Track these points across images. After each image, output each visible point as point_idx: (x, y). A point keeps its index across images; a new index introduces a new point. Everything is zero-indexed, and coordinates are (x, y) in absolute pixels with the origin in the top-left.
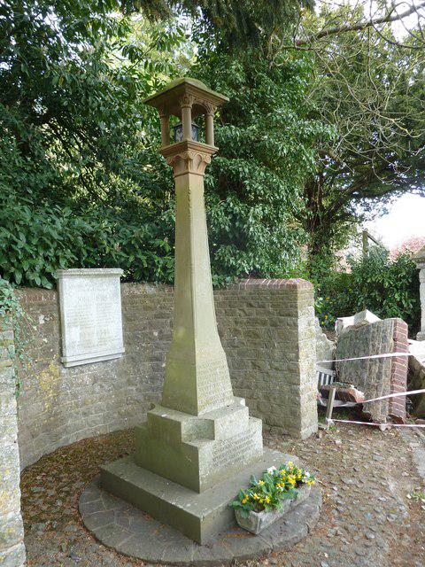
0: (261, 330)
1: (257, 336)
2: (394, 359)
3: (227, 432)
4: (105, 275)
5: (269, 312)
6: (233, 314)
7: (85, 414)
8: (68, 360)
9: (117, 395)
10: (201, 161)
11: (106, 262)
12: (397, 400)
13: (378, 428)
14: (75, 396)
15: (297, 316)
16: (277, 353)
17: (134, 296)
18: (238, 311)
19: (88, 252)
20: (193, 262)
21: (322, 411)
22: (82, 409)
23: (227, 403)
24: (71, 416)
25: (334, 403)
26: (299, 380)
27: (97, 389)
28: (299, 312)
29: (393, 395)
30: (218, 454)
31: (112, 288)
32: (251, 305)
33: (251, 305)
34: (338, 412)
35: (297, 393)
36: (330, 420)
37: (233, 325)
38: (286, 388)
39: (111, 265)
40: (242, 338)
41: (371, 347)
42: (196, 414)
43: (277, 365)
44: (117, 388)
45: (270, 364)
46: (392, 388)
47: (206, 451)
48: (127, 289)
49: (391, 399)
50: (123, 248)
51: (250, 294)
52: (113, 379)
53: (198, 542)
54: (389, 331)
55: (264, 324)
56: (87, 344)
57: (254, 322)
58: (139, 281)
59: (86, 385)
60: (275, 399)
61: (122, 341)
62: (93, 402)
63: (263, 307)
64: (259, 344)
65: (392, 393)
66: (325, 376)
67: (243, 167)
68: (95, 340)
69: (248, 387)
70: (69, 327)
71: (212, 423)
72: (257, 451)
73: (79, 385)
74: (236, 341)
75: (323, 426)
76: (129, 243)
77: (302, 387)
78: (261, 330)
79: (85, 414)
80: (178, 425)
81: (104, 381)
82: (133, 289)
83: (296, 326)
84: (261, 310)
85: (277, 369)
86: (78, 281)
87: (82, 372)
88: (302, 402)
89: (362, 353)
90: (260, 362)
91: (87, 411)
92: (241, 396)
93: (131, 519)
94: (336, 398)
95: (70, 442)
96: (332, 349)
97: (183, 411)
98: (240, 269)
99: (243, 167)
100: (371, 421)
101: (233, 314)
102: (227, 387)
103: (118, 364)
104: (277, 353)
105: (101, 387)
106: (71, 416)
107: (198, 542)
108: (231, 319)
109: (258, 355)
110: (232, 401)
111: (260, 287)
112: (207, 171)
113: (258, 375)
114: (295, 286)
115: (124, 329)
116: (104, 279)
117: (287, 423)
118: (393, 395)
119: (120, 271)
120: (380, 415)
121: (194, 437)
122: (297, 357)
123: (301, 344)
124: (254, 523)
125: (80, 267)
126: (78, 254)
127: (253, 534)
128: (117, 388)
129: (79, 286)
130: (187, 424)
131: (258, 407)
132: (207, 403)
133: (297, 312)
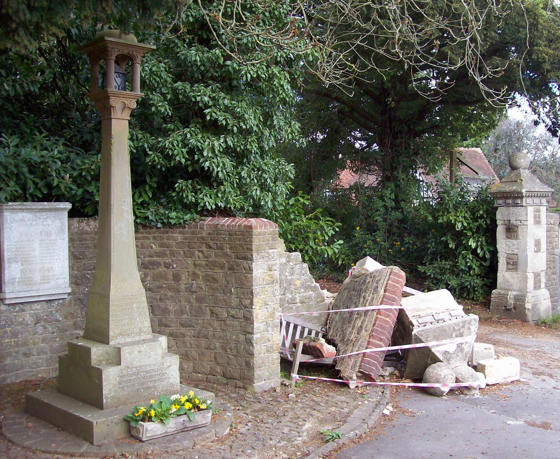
0: (219, 274)
1: (215, 280)
2: (379, 311)
3: (141, 356)
4: (50, 210)
5: (227, 255)
6: (192, 255)
7: (25, 354)
8: (7, 296)
9: (61, 338)
10: (125, 107)
11: (51, 195)
12: (370, 356)
13: (346, 385)
14: (15, 334)
15: (252, 260)
16: (234, 301)
17: (83, 233)
18: (197, 253)
19: (36, 184)
20: (112, 203)
21: (286, 365)
22: (23, 349)
23: (143, 337)
24: (10, 354)
25: (300, 358)
26: (253, 328)
27: (40, 329)
28: (255, 255)
29: (367, 351)
30: (125, 379)
31: (58, 223)
32: (210, 247)
33: (210, 247)
34: (305, 368)
35: (250, 342)
36: (295, 375)
37: (191, 268)
38: (242, 338)
39: (59, 199)
40: (200, 282)
41: (362, 300)
42: (108, 343)
43: (233, 312)
44: (63, 330)
45: (228, 312)
46: (369, 343)
47: (111, 378)
48: (76, 225)
49: (364, 353)
50: (74, 180)
51: (209, 234)
52: (57, 321)
53: (92, 443)
54: (382, 281)
55: (222, 267)
56: (27, 280)
57: (212, 265)
58: (91, 216)
59: (27, 324)
60: (231, 349)
61: (67, 280)
62: (34, 343)
63: (222, 249)
64: (217, 289)
65: (367, 348)
66: (295, 327)
67: (203, 94)
68: (37, 277)
69: (206, 337)
70: (9, 262)
71: (119, 350)
72: (172, 385)
73: (20, 324)
74: (194, 285)
75: (287, 382)
76: (80, 175)
77: (255, 336)
78: (219, 274)
79: (25, 354)
80: (88, 351)
81: (46, 321)
82: (83, 224)
83: (251, 270)
84: (219, 252)
85: (233, 317)
86: (20, 215)
87: (24, 311)
88: (256, 353)
89: (354, 306)
90: (218, 310)
91: (28, 352)
92: (160, 333)
93: (43, 431)
94: (303, 352)
95: (8, 381)
96: (328, 301)
97: (94, 340)
98: (202, 204)
99: (203, 94)
100: (341, 378)
101: (192, 255)
102: (144, 321)
103: (63, 305)
104: (234, 301)
105: (45, 328)
106: (10, 354)
107: (92, 443)
108: (190, 261)
109: (216, 301)
110: (150, 336)
111: (219, 226)
112: (132, 115)
113: (216, 323)
114: (251, 227)
115: (71, 268)
116: (49, 214)
117: (242, 375)
118: (367, 351)
119: (69, 206)
120: (349, 371)
121: (104, 362)
122: (252, 304)
123: (256, 289)
124: (141, 431)
125: (26, 200)
126: (24, 188)
127: (141, 441)
128: (63, 330)
129: (22, 220)
130: (97, 352)
131: (215, 358)
132: (121, 334)
133: (252, 255)
